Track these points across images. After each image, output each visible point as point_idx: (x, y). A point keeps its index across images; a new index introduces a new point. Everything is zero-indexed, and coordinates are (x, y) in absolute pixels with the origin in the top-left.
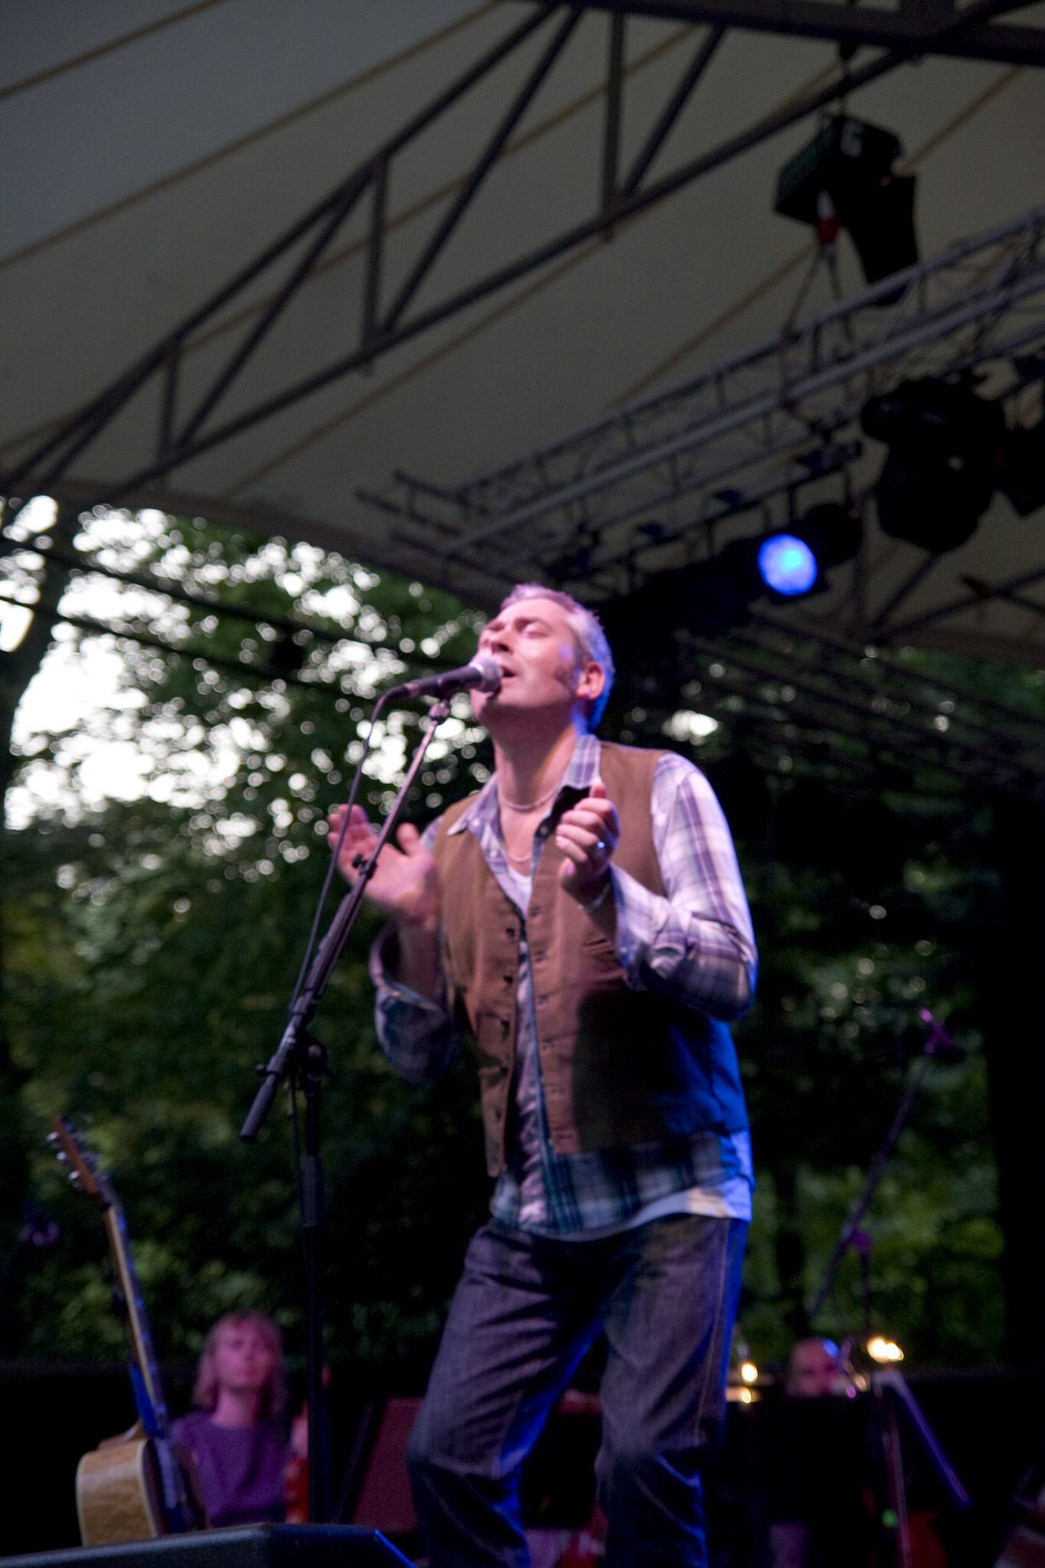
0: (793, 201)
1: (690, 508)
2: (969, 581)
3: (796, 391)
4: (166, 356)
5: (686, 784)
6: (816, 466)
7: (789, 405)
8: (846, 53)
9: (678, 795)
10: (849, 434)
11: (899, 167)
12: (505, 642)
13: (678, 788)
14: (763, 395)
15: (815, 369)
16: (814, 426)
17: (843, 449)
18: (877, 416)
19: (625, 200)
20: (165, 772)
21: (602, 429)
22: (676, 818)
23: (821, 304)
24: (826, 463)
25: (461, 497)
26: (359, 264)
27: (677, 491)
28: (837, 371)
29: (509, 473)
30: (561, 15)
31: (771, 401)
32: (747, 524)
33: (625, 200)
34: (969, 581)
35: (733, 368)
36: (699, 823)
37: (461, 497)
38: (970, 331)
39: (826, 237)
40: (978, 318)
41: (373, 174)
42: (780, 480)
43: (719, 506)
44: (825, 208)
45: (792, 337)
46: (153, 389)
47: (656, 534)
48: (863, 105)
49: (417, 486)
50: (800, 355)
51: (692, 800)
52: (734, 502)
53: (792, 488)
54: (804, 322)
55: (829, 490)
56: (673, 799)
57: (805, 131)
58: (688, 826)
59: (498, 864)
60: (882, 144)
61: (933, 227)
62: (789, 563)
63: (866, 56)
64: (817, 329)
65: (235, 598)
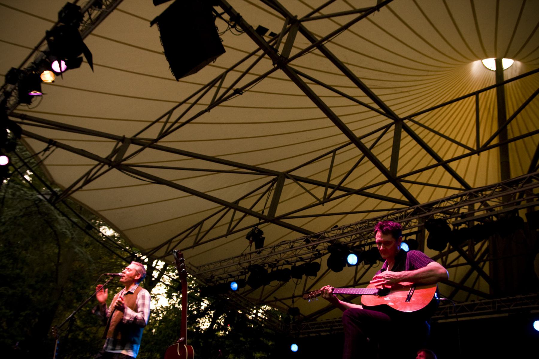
0: (248, 237)
2: (275, 297)
4: (169, 242)
6: (242, 273)
7: (240, 264)
8: (260, 220)
11: (263, 236)
16: (243, 268)
19: (230, 232)
21: (229, 259)
23: (248, 251)
25: (197, 268)
26: (202, 231)
27: (225, 273)
29: (204, 266)
30: (228, 208)
32: (230, 280)
33: (230, 232)
34: (275, 297)
37: (197, 268)
39: (251, 243)
41: (201, 223)
43: (229, 276)
44: (251, 239)
46: (166, 246)
47: (221, 279)
48: (259, 227)
49: (192, 265)
52: (231, 276)
53: (239, 276)
54: (244, 253)
55: (243, 277)
57: (251, 229)
60: (261, 232)
61: (265, 243)
62: (235, 286)
63: (262, 221)
65: (345, 296)
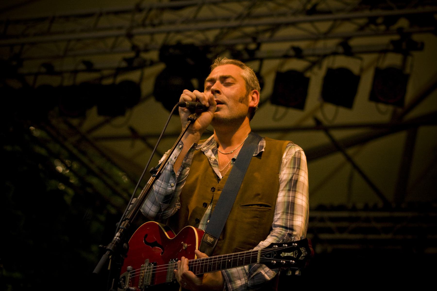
1: (68, 64)
3: (135, 31)
5: (299, 152)
9: (295, 155)
10: (154, 55)
12: (218, 89)
13: (296, 152)
14: (120, 28)
15: (143, 25)
16: (134, 48)
17: (145, 61)
18: (165, 51)
20: (247, 91)
22: (291, 162)
24: (135, 64)
28: (150, 29)
31: (123, 32)
35: (108, 13)
36: (299, 168)
38: (216, 32)
40: (222, 28)
42: (116, 65)
45: (139, 9)
50: (139, 17)
51: (300, 159)
56: (293, 155)
58: (294, 168)
59: (214, 163)
64: (150, 9)
